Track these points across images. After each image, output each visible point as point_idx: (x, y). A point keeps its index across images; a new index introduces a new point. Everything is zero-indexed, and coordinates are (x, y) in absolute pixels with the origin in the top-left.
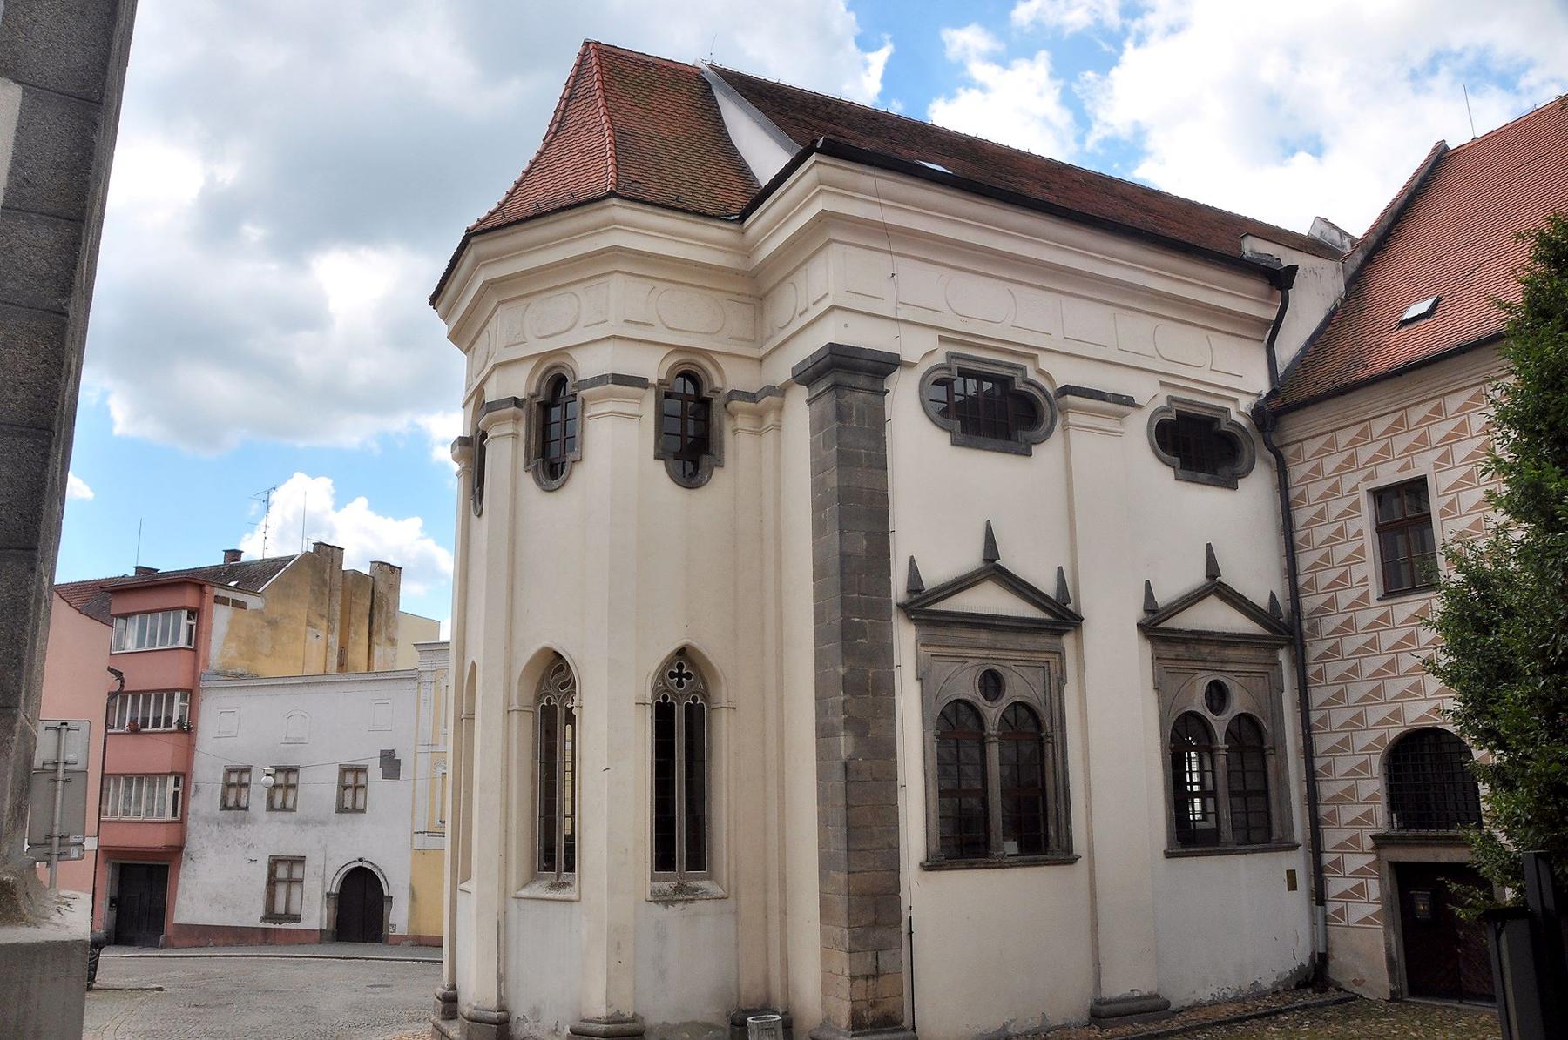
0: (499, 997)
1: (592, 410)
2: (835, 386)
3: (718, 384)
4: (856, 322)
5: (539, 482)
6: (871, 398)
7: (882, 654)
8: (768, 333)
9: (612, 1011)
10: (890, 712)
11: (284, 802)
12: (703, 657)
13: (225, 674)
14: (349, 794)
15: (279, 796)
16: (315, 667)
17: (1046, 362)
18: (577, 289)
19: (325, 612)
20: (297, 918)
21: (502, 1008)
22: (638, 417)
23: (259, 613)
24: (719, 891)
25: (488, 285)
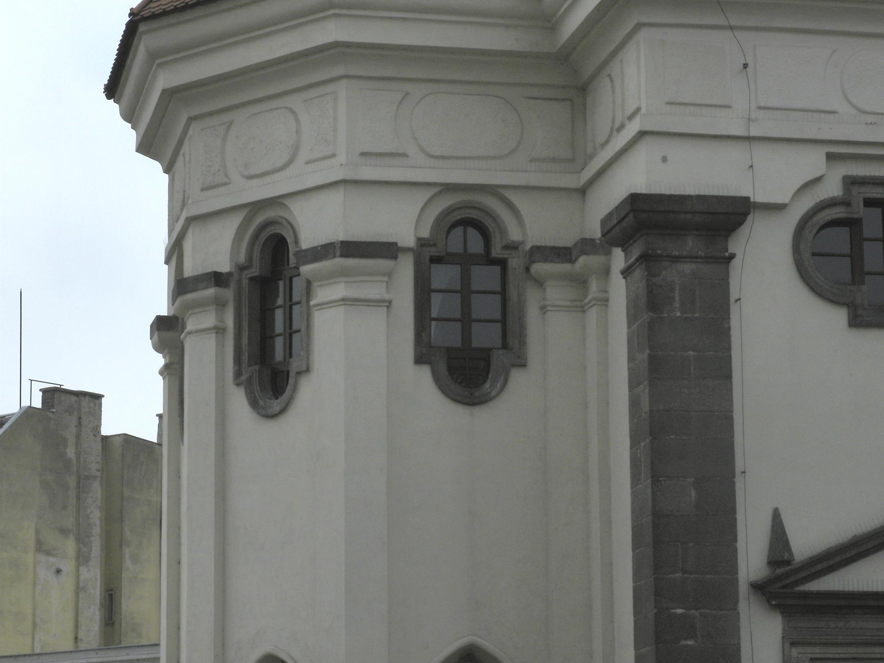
1: (322, 294)
2: (645, 258)
3: (515, 235)
4: (678, 151)
5: (254, 404)
19: (70, 523)
22: (389, 304)
25: (170, 95)
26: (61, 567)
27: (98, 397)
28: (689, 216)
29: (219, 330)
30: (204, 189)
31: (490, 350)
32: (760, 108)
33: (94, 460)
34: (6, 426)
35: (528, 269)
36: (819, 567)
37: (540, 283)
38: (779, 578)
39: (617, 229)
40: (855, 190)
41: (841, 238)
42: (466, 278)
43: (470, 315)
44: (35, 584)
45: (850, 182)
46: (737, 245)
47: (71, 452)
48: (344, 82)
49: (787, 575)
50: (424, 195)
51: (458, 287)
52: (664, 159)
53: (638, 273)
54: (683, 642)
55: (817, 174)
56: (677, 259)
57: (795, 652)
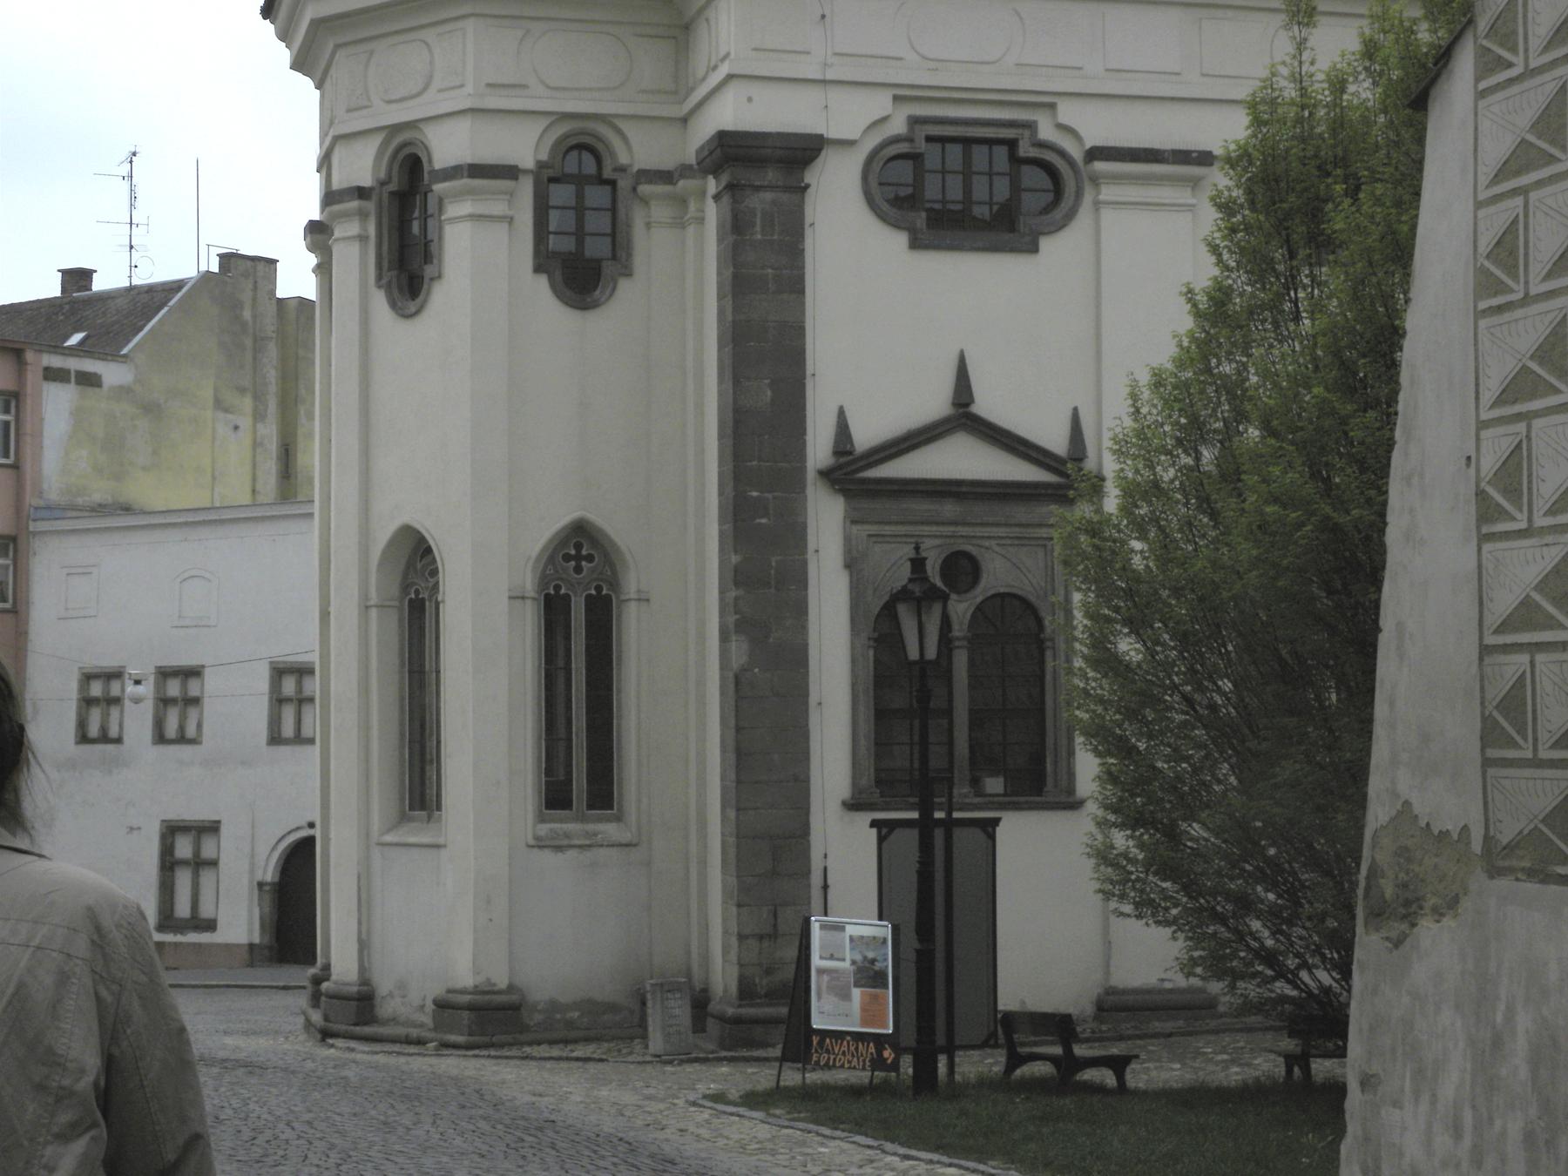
0: (363, 969)
1: (453, 210)
2: (731, 187)
3: (623, 159)
5: (393, 305)
6: (785, 197)
7: (793, 536)
8: (700, 73)
9: (480, 979)
10: (801, 610)
11: (182, 728)
12: (600, 530)
13: (74, 508)
14: (288, 714)
15: (95, 716)
16: (235, 490)
17: (1068, 113)
18: (429, 35)
20: (211, 926)
21: (365, 981)
23: (123, 391)
24: (626, 837)
25: (316, 24)
26: (239, 423)
27: (274, 262)
29: (362, 238)
30: (349, 111)
31: (599, 261)
32: (836, 54)
33: (269, 325)
34: (184, 290)
35: (634, 189)
36: (876, 457)
37: (645, 201)
40: (917, 127)
41: (905, 170)
42: (580, 196)
43: (581, 234)
44: (214, 439)
45: (914, 121)
46: (811, 176)
47: (247, 314)
48: (471, 21)
49: (849, 464)
50: (543, 123)
51: (573, 204)
52: (750, 100)
53: (726, 199)
55: (885, 114)
56: (758, 188)
57: (855, 529)
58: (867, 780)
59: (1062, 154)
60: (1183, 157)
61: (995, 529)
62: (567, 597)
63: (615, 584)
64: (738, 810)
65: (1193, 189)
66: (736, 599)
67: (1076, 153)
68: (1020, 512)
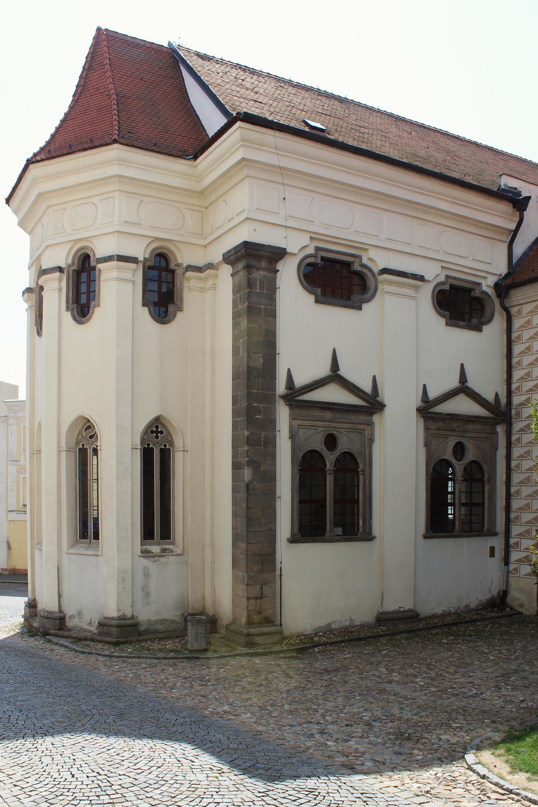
0: (60, 606)
4: (260, 227)
6: (269, 274)
7: (270, 424)
17: (373, 253)
21: (61, 611)
28: (264, 253)
35: (184, 274)
36: (303, 391)
38: (290, 394)
39: (233, 257)
40: (318, 252)
42: (160, 276)
45: (317, 249)
46: (280, 266)
52: (255, 230)
54: (257, 416)
56: (259, 269)
57: (293, 422)
58: (296, 530)
59: (370, 270)
60: (414, 277)
61: (344, 425)
62: (152, 449)
63: (172, 444)
64: (248, 544)
65: (416, 291)
66: (248, 451)
67: (376, 270)
68: (353, 417)
